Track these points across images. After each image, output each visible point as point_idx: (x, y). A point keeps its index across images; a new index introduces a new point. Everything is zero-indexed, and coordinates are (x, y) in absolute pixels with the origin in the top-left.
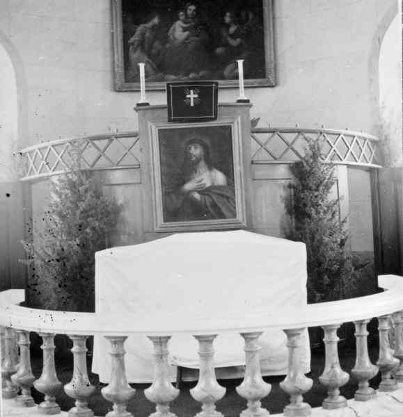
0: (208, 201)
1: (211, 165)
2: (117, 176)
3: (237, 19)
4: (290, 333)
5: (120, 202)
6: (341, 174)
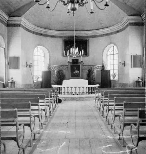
0: (77, 75)
1: (77, 70)
2: (64, 71)
3: (83, 46)
4: (87, 87)
5: (65, 74)
6: (96, 71)
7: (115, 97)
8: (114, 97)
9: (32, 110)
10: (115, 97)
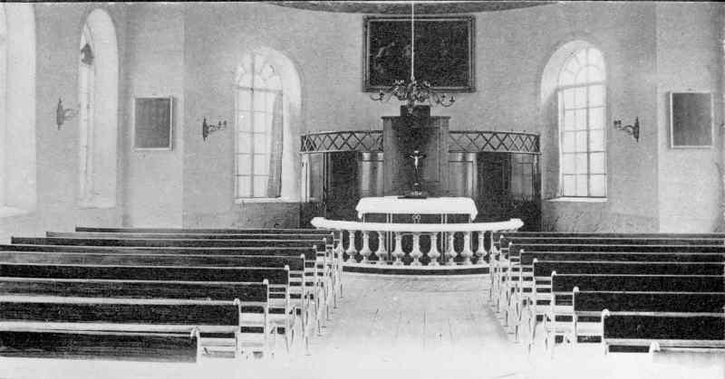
7: (535, 260)
8: (532, 261)
9: (245, 330)
10: (535, 260)
